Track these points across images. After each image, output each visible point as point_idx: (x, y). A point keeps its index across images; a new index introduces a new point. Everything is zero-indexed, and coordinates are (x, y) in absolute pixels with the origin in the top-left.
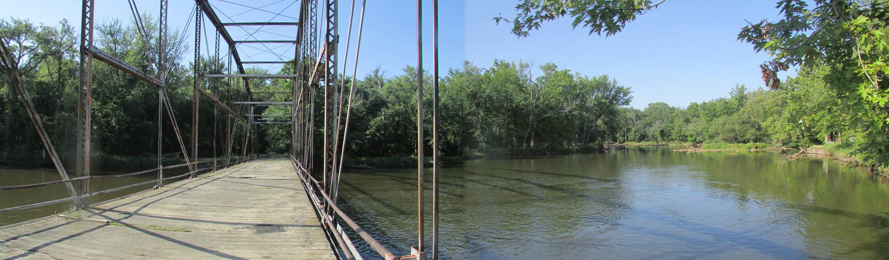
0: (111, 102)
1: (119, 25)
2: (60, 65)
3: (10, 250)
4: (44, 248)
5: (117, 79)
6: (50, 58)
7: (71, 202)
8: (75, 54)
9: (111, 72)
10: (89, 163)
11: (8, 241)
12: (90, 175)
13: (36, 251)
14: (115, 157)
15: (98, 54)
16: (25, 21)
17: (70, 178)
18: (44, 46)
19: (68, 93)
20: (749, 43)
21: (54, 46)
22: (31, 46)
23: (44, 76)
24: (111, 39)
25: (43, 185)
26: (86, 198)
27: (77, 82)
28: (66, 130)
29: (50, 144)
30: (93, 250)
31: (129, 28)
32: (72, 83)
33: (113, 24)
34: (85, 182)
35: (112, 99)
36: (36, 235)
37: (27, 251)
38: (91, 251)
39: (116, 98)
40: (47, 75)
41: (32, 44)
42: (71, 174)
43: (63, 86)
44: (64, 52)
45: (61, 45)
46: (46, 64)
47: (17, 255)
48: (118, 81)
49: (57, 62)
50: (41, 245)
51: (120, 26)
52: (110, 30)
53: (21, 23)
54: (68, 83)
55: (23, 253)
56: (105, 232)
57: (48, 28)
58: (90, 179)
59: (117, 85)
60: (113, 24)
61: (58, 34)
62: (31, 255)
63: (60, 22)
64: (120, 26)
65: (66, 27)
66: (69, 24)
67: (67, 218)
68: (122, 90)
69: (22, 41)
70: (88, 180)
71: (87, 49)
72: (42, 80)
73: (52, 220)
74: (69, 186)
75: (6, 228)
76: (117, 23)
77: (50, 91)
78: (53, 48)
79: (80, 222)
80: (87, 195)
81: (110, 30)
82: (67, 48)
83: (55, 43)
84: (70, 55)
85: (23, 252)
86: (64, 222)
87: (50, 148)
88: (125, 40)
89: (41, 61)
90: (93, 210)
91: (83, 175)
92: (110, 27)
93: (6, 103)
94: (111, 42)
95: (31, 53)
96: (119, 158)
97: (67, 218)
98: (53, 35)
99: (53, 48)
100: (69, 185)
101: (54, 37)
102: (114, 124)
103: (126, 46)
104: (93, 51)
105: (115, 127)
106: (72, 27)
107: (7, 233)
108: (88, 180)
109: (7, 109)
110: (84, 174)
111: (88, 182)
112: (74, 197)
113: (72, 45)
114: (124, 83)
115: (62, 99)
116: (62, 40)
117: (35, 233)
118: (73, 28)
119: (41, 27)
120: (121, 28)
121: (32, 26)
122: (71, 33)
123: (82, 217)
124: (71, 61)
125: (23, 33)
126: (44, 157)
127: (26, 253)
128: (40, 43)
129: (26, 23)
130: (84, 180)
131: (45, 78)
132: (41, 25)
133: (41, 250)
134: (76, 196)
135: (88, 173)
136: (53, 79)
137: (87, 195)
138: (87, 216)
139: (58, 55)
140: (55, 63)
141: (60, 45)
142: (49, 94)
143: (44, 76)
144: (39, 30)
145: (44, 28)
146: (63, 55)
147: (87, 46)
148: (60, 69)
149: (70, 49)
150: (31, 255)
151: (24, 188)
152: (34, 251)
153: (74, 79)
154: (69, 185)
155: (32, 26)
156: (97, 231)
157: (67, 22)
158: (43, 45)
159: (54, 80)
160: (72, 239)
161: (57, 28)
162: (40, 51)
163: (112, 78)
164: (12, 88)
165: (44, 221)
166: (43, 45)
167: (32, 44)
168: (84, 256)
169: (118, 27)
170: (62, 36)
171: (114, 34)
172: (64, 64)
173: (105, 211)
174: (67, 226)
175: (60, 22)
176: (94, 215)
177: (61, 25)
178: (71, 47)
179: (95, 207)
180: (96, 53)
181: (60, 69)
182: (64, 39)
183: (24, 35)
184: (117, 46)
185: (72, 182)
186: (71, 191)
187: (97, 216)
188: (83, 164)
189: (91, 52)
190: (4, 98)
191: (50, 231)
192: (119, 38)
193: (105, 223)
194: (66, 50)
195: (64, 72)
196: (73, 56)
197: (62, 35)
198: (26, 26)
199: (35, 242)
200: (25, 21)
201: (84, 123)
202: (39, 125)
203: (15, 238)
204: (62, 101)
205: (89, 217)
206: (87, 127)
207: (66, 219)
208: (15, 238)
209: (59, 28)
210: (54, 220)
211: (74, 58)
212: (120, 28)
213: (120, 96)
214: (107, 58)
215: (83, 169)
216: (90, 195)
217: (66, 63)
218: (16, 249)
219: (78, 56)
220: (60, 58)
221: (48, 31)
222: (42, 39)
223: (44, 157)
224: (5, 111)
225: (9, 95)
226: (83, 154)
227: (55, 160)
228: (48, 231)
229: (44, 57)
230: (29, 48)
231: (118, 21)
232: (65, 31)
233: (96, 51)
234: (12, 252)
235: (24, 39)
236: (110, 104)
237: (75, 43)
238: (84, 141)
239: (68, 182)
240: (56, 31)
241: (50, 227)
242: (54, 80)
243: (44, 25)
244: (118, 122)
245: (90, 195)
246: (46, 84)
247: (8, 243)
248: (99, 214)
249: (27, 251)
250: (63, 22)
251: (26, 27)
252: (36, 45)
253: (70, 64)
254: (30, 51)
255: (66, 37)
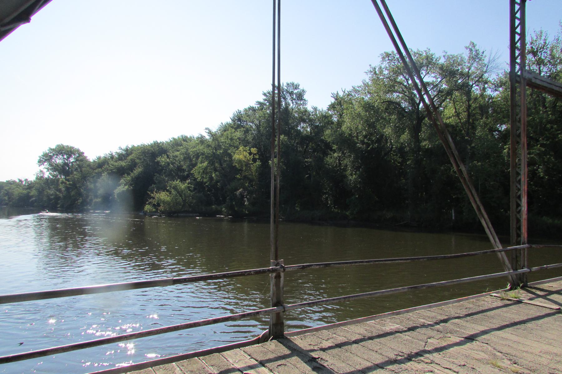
0: (538, 145)
1: (543, 38)
2: (469, 101)
3: (441, 335)
4: (483, 337)
5: (544, 112)
6: (457, 93)
7: (505, 278)
8: (486, 86)
9: (535, 104)
10: (526, 227)
11: (437, 324)
12: (528, 243)
13: (474, 340)
14: (545, 218)
15: (533, 80)
16: (425, 51)
17: (503, 247)
18: (449, 80)
19: (480, 137)
20: (264, 96)
21: (460, 78)
22: (433, 81)
23: (450, 118)
24: (533, 59)
25: (473, 255)
26: (523, 273)
27: (490, 122)
28: (480, 183)
29: (479, 203)
30: (547, 346)
31: (558, 40)
32: (485, 123)
33: (535, 39)
34: (522, 252)
35: (537, 141)
36: (468, 318)
37: (463, 339)
38: (546, 347)
39: (543, 139)
40: (453, 115)
41: (434, 79)
42: (505, 241)
43: (474, 128)
44: (472, 85)
45: (469, 77)
46: (452, 102)
47: (451, 343)
48: (545, 115)
49: (464, 98)
50: (478, 332)
51: (545, 40)
52: (532, 47)
53: (421, 55)
54: (479, 123)
55: (458, 341)
56: (558, 323)
57: (453, 57)
58: (528, 248)
59: (544, 120)
60: (535, 39)
61: (465, 63)
62: (468, 345)
63: (466, 48)
64: (545, 40)
65: (474, 53)
66: (477, 48)
67: (503, 299)
68: (552, 128)
69: (422, 76)
70: (526, 249)
71: (519, 76)
72: (448, 121)
73: (484, 301)
74: (502, 256)
75: (430, 307)
76: (541, 36)
77: (457, 136)
78: (460, 81)
79: (520, 305)
80: (525, 269)
81: (532, 47)
82: (477, 79)
83: (462, 74)
84: (480, 88)
85: (458, 340)
86: (500, 303)
87: (478, 207)
88: (553, 57)
89: (446, 98)
90: (534, 290)
91: (518, 243)
92: (531, 43)
93: (407, 152)
94: (534, 64)
95: (434, 89)
96: (550, 221)
97: (503, 299)
98: (459, 65)
99: (460, 81)
100: (503, 256)
101: (459, 68)
102: (542, 175)
103: (555, 65)
104: (526, 77)
105: (543, 178)
106: (481, 51)
107: (433, 314)
108: (526, 249)
109: (409, 160)
110: (520, 241)
111: (526, 253)
112: (507, 272)
113: (482, 75)
114: (554, 117)
115: (473, 145)
116: (469, 70)
117: (467, 315)
118: (483, 53)
119: (444, 56)
120: (547, 42)
121: (434, 56)
122: (480, 60)
123: (521, 298)
124: (482, 95)
125: (424, 66)
126: (453, 218)
127: (462, 341)
128: (444, 77)
129: (426, 53)
130: (520, 250)
131: (450, 119)
132: (444, 54)
133: (479, 338)
134: (512, 271)
135: (526, 240)
136: (460, 119)
137: (525, 269)
138: (529, 297)
139: (466, 89)
140: (462, 99)
141: (468, 75)
142: (456, 139)
143: (450, 118)
144: (442, 61)
145: (448, 57)
146: (472, 89)
147: (518, 72)
148: (469, 106)
149: (480, 80)
150: (468, 344)
151: (451, 257)
152: (471, 338)
153: (487, 118)
154: (503, 256)
155: (434, 56)
156: (546, 319)
157: (474, 47)
158: (448, 78)
159: (462, 121)
160: (515, 327)
161: (463, 56)
162: (444, 86)
163: (538, 112)
164: (414, 135)
165: (474, 300)
166: (448, 78)
167: (434, 79)
168: (537, 353)
169: (542, 42)
170: (469, 65)
171: (537, 51)
172: (473, 100)
173: (551, 293)
174: (504, 309)
175: (466, 48)
176: (537, 298)
177: (468, 51)
178: (481, 77)
179: (536, 286)
180: (530, 80)
181: (469, 106)
182: (472, 68)
183: (425, 68)
184: (541, 68)
185: (506, 252)
186: (504, 264)
187: (540, 299)
188: (519, 228)
189: (524, 79)
190: (406, 146)
191: (485, 314)
192: (544, 55)
193: (555, 311)
194: (475, 82)
195: (474, 110)
196: (484, 89)
197: (469, 63)
198: (427, 58)
199: (471, 328)
200: (425, 51)
201: (518, 174)
202: (464, 179)
203: (445, 321)
204: (473, 147)
205: (530, 299)
206: (522, 180)
207: (501, 300)
208: (445, 321)
209: (466, 55)
210: (486, 299)
211: (485, 92)
212: (545, 43)
213: (548, 135)
214: (545, 84)
215: (519, 235)
216: (529, 270)
217: (476, 99)
218: (449, 335)
219: (490, 88)
220: (468, 93)
221: (454, 61)
222: (447, 71)
223: (453, 218)
224: (406, 162)
225: (410, 144)
226: (518, 216)
227: (485, 223)
228: (483, 314)
229: (449, 93)
230: (431, 83)
231: (541, 33)
232: (473, 57)
233: (530, 76)
234: (445, 339)
235: (425, 74)
236: (535, 147)
237: (486, 72)
238: (519, 197)
239: (500, 251)
240: (462, 60)
241: (484, 309)
242: (462, 121)
243: (448, 54)
244: (546, 172)
245: (529, 270)
246: (452, 126)
247: (438, 326)
248: (544, 297)
249: (463, 339)
250: (470, 47)
251: (427, 59)
252: (439, 80)
253: (480, 99)
254: (433, 88)
255: (475, 65)
